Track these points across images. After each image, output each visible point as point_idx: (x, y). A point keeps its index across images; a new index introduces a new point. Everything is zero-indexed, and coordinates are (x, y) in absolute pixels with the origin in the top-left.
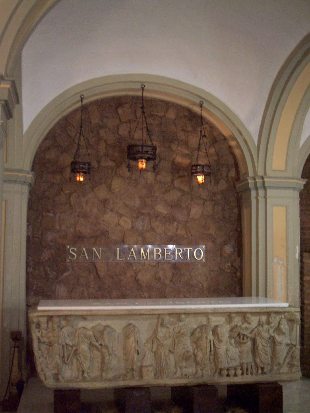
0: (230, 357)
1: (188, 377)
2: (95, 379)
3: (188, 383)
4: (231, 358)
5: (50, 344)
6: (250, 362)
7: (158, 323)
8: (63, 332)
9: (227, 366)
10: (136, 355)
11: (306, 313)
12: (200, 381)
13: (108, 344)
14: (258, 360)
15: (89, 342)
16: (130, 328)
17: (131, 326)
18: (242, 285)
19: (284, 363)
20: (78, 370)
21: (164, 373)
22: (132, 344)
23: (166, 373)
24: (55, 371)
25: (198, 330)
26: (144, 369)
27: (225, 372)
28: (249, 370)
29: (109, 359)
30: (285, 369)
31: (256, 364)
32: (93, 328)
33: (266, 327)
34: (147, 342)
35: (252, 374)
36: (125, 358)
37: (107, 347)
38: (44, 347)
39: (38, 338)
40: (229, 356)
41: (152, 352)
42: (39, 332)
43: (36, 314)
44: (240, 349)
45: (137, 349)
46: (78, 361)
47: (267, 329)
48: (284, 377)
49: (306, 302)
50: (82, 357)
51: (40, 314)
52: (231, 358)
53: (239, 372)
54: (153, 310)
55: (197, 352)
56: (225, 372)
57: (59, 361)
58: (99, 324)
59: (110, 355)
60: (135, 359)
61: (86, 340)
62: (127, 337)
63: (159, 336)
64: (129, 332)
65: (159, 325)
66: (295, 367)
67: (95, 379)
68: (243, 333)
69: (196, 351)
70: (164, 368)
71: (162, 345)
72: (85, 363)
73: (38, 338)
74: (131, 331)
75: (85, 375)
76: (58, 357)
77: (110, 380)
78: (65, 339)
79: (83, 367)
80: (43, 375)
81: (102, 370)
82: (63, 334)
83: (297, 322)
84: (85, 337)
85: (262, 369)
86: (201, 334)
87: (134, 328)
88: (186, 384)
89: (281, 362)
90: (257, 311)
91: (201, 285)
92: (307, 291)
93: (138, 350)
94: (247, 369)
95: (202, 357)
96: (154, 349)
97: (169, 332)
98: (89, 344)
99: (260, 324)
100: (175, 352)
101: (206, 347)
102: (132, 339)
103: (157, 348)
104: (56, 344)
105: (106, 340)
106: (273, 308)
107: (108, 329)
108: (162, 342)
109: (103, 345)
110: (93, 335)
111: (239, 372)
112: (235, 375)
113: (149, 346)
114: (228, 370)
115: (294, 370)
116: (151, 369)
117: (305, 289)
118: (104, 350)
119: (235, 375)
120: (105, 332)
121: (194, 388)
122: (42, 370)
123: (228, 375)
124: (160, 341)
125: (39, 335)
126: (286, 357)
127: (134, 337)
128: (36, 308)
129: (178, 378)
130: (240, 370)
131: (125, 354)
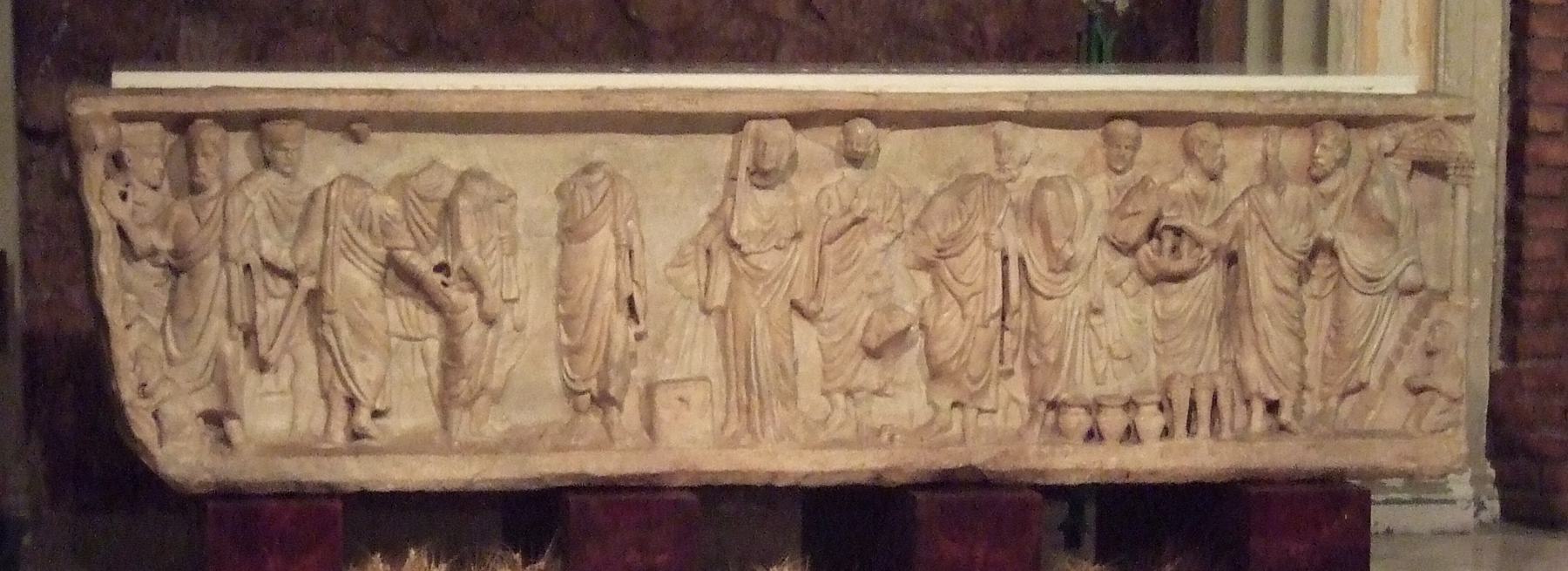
0: (1104, 344)
1: (892, 438)
2: (415, 445)
3: (887, 470)
4: (1110, 350)
5: (179, 266)
6: (1211, 374)
7: (733, 164)
8: (248, 201)
9: (1090, 391)
10: (620, 321)
11: (1534, 182)
12: (949, 459)
13: (478, 262)
14: (1251, 365)
15: (380, 252)
16: (590, 187)
17: (598, 176)
18: (1193, 33)
19: (1383, 380)
20: (326, 396)
21: (768, 419)
22: (602, 264)
23: (778, 425)
24: (206, 401)
25: (944, 203)
26: (661, 397)
27: (1077, 420)
28: (1204, 410)
29: (482, 341)
30: (1391, 411)
31: (1240, 379)
32: (400, 185)
33: (1296, 192)
34: (679, 261)
35: (1215, 430)
36: (565, 339)
37: (472, 281)
38: (147, 276)
39: (122, 233)
40: (1099, 341)
41: (706, 311)
42: (124, 196)
43: (109, 105)
44: (1157, 303)
45: (626, 295)
46: (324, 350)
47: (1303, 203)
48: (1383, 455)
49: (1539, 119)
50: (345, 332)
51: (130, 105)
52: (1110, 350)
53: (1150, 420)
54: (710, 93)
55: (938, 317)
56: (1077, 420)
57: (229, 348)
58: (433, 163)
59: (490, 321)
60: (618, 338)
61: (366, 243)
62: (571, 232)
63: (740, 225)
64: (587, 209)
65: (742, 174)
66: (1442, 402)
67: (415, 445)
68: (1177, 223)
69: (931, 310)
70: (765, 387)
71: (757, 276)
72: (363, 359)
73: (122, 233)
74: (597, 201)
75: (363, 418)
76: (218, 323)
77: (493, 450)
78: (257, 238)
79: (351, 384)
80: (149, 416)
81: (446, 402)
82: (245, 209)
83: (1458, 172)
84: (360, 227)
85: (1272, 407)
86: (959, 224)
87: (613, 183)
88: (878, 475)
89: (1373, 375)
90: (1252, 108)
91: (970, 27)
92: (1546, 60)
93: (631, 300)
94: (1089, 50)
95: (961, 341)
96: (718, 299)
97: (796, 207)
98: (383, 259)
99: (1271, 175)
100: (822, 315)
101: (985, 290)
102: (603, 239)
103: (732, 292)
104: (213, 261)
105: (468, 240)
106: (1338, 96)
107: (479, 188)
108: (753, 259)
109: (455, 267)
110: (399, 216)
111: (1150, 420)
112: (1131, 434)
113: (691, 278)
114: (1095, 407)
115: (1433, 416)
116: (696, 394)
117: (1533, 52)
118: (457, 295)
119: (1131, 434)
120: (463, 202)
121: (920, 496)
122: (143, 390)
123: (1093, 435)
124: (744, 255)
125: (122, 211)
126: (1399, 353)
127: (615, 231)
128: (105, 79)
129: (840, 444)
130: (1154, 408)
131: (567, 320)
